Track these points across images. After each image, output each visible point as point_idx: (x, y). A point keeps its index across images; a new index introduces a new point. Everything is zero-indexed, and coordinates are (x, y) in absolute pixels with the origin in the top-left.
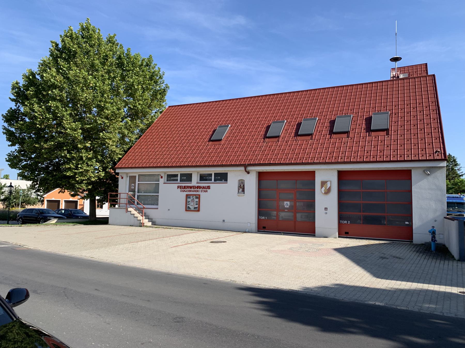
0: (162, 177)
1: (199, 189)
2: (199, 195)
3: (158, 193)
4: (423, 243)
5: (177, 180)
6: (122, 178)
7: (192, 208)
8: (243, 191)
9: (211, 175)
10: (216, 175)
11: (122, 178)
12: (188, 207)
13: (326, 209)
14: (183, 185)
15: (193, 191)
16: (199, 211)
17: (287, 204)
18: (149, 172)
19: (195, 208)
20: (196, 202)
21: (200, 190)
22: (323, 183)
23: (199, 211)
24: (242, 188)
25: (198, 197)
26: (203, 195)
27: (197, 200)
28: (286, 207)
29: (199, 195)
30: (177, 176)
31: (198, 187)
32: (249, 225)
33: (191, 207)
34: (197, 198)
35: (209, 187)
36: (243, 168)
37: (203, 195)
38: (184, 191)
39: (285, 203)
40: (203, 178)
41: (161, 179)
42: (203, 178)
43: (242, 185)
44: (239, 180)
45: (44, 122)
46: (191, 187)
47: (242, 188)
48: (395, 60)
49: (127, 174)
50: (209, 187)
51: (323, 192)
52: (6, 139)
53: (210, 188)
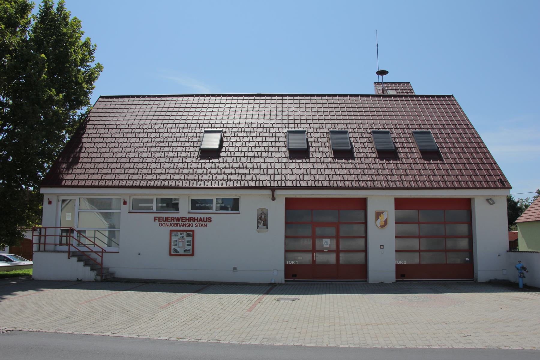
0: (125, 203)
1: (192, 222)
2: (193, 231)
3: (119, 228)
4: (487, 281)
5: (210, 208)
6: (50, 203)
7: (181, 251)
8: (266, 225)
9: (151, 201)
10: (163, 200)
11: (50, 203)
12: (175, 250)
13: (382, 246)
14: (165, 215)
15: (182, 225)
16: (192, 255)
17: (326, 242)
18: (102, 195)
19: (185, 251)
20: (188, 241)
21: (194, 223)
22: (378, 214)
23: (192, 255)
24: (263, 220)
25: (191, 234)
26: (199, 231)
27: (190, 239)
28: (325, 246)
29: (193, 231)
30: (151, 201)
31: (190, 219)
32: (275, 273)
33: (178, 249)
34: (188, 235)
35: (209, 220)
36: (269, 192)
37: (199, 231)
38: (166, 225)
39: (324, 240)
40: (196, 204)
41: (123, 206)
42: (196, 204)
43: (263, 217)
44: (262, 209)
45: (34, 33)
46: (178, 219)
47: (263, 220)
48: (382, 73)
49: (58, 195)
50: (209, 220)
51: (379, 226)
52: (82, 24)
53: (211, 221)
